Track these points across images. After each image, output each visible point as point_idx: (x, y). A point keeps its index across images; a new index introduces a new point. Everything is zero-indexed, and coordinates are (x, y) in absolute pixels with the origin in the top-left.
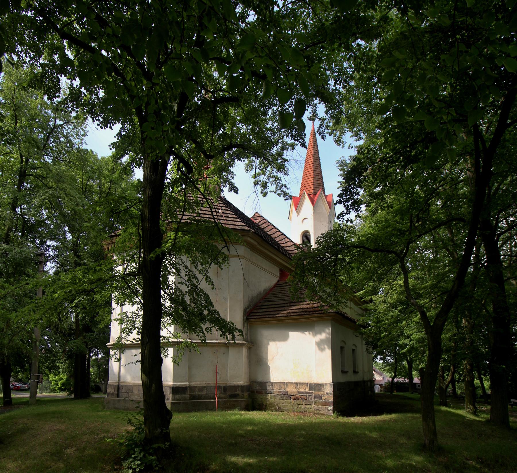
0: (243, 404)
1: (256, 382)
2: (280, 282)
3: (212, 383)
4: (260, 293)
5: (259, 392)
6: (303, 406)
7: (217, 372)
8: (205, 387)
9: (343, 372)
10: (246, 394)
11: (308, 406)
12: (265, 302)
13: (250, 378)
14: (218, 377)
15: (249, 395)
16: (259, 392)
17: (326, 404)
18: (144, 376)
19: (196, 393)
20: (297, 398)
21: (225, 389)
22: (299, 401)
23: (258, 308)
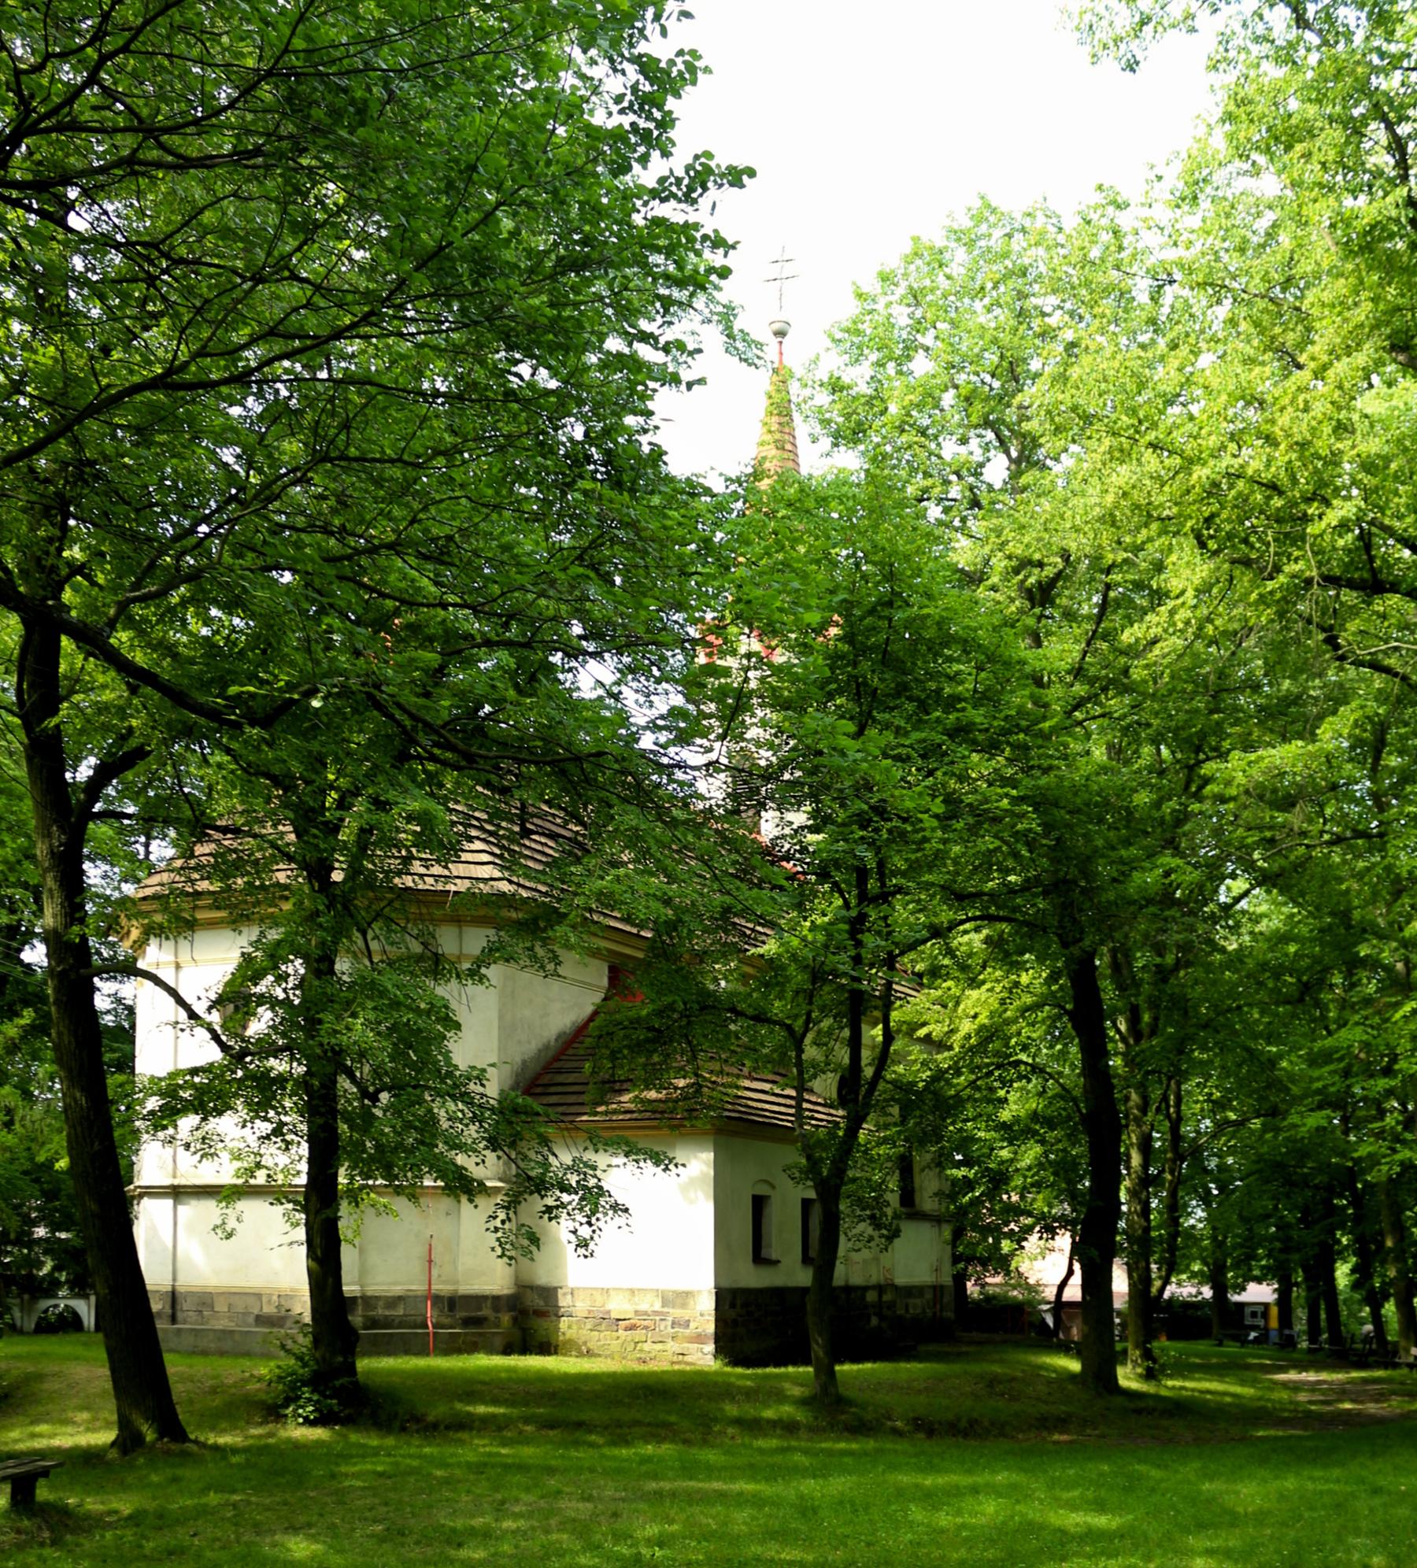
0: (498, 1342)
1: (532, 1288)
2: (611, 1004)
3: (419, 1287)
4: (547, 1047)
5: (541, 1314)
6: (646, 1347)
7: (430, 1261)
8: (400, 1298)
9: (759, 1258)
10: (506, 1319)
11: (659, 1346)
12: (559, 1072)
13: (517, 1277)
14: (435, 1272)
15: (515, 1320)
16: (541, 1314)
17: (699, 1339)
18: (314, 1265)
19: (381, 1311)
20: (632, 1328)
21: (451, 1303)
22: (639, 1334)
23: (539, 1090)
